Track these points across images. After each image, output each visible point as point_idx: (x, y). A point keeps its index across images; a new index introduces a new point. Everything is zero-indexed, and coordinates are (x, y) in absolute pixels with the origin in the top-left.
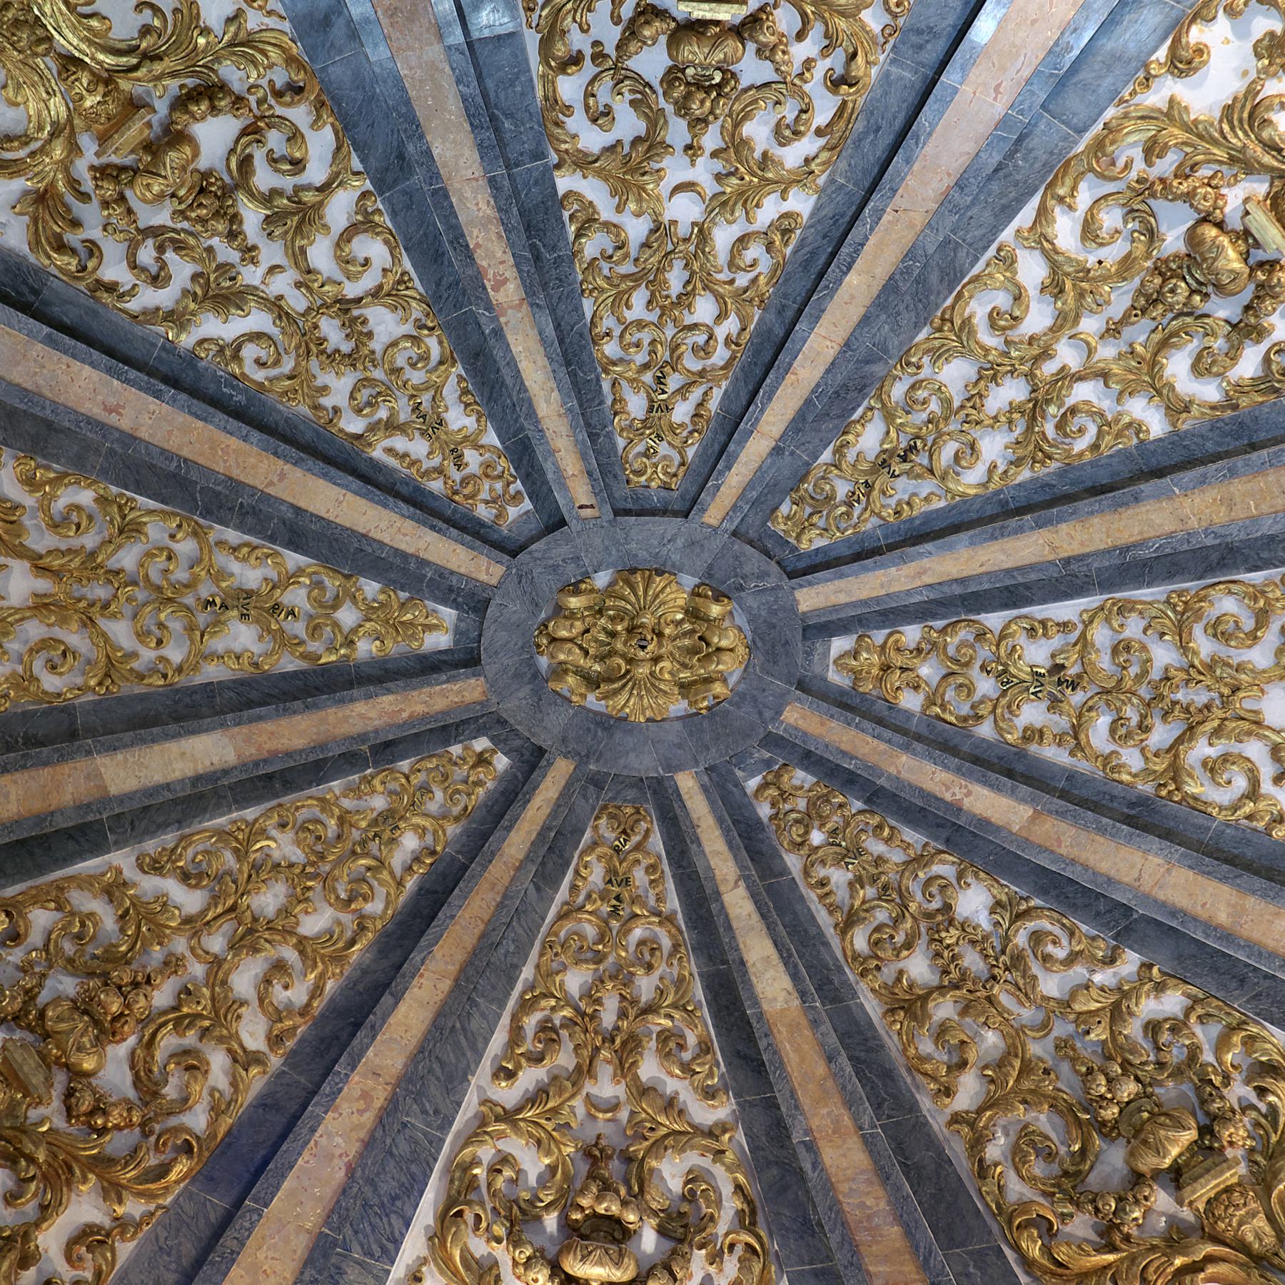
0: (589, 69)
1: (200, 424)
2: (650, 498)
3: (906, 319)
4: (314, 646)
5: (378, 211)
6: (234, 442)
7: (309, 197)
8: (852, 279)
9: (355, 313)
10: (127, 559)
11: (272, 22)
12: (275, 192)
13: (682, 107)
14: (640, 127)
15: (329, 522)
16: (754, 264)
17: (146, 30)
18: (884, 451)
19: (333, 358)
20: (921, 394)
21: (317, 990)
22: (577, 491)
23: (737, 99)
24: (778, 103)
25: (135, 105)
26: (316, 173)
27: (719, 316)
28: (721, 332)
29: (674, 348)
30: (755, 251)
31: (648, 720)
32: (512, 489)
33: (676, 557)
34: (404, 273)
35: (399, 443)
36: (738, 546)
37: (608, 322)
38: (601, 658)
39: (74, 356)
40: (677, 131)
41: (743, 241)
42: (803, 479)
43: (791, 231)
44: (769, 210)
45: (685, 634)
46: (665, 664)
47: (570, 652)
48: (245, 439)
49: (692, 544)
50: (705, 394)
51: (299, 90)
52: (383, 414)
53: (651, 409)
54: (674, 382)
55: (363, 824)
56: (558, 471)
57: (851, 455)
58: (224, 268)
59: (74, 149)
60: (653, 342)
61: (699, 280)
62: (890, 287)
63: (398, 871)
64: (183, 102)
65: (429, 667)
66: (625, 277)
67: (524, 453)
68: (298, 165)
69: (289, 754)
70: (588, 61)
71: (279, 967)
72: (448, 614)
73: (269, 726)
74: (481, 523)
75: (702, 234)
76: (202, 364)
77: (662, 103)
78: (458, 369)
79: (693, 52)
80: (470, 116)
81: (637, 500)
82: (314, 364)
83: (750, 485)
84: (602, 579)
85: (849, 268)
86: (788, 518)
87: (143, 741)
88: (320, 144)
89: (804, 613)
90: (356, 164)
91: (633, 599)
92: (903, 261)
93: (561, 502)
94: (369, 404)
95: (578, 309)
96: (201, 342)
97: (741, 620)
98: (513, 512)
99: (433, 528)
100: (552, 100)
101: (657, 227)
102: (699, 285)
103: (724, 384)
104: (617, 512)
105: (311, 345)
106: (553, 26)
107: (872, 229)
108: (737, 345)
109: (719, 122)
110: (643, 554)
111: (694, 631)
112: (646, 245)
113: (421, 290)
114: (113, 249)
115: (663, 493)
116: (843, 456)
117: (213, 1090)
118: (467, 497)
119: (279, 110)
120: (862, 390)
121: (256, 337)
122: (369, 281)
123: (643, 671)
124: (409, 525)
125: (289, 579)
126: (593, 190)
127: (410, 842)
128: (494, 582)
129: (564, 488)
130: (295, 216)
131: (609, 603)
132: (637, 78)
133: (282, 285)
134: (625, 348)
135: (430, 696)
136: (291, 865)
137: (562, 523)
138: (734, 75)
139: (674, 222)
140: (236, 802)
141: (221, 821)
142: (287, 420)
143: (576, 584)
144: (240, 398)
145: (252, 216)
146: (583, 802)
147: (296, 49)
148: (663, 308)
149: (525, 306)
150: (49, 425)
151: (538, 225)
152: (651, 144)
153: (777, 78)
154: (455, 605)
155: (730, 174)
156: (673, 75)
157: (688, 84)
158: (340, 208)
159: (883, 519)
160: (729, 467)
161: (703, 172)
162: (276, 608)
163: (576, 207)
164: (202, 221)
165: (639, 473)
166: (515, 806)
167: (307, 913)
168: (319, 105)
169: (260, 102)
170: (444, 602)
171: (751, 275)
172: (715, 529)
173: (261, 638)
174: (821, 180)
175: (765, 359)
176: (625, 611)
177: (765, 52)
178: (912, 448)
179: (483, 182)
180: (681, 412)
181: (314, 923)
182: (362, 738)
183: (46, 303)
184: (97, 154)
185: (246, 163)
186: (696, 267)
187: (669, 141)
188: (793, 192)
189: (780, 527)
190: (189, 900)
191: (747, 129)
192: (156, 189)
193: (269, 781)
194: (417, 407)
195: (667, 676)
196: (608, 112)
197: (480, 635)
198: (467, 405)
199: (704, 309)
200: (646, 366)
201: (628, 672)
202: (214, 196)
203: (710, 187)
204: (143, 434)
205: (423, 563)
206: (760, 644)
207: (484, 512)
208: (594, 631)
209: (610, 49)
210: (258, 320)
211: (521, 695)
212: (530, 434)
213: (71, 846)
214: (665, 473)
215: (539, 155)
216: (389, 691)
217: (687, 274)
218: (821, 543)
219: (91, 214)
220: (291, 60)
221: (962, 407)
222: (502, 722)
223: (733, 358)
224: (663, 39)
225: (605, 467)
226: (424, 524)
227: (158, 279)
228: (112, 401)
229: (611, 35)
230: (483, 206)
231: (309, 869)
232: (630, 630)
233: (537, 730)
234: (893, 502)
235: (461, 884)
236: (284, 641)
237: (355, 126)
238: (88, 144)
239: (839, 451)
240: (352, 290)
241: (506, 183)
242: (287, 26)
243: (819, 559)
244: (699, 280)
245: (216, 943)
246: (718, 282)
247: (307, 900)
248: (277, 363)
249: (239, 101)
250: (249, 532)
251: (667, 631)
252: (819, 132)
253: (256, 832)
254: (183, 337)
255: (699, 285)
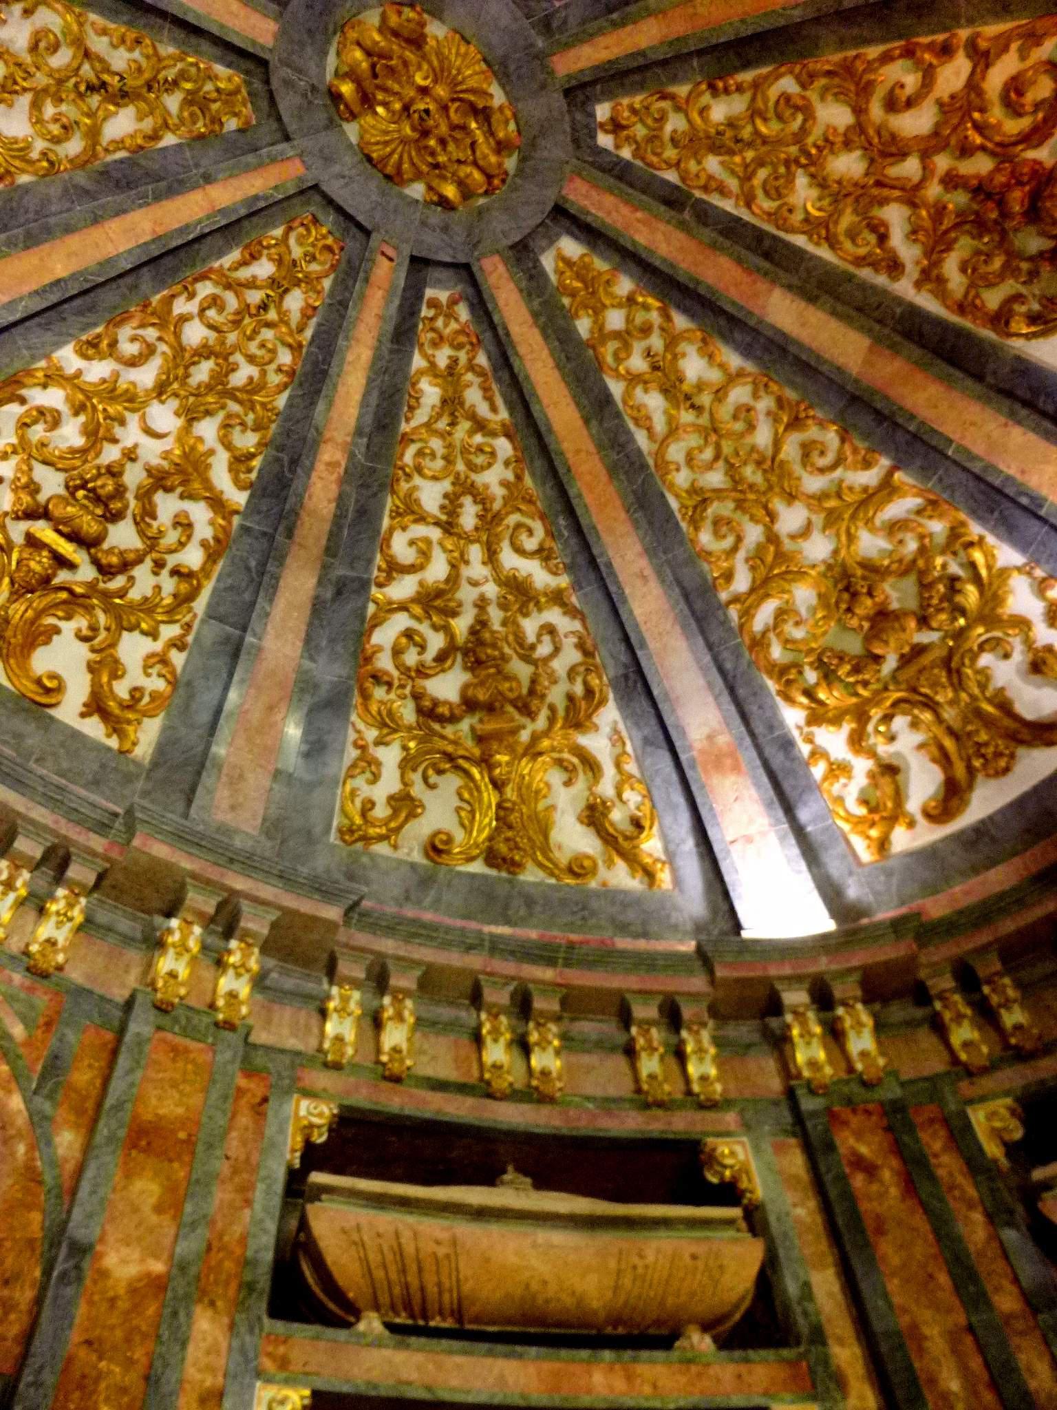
0: (172, 561)
1: (599, 527)
2: (335, 223)
3: (31, 202)
4: (655, 317)
5: (380, 569)
6: (588, 499)
7: (417, 610)
8: (60, 269)
9: (444, 518)
10: (716, 478)
11: (361, 726)
12: (435, 628)
13: (120, 492)
14: (159, 498)
15: (574, 397)
16: (133, 339)
17: (440, 772)
18: (117, 105)
19: (481, 499)
20: (56, 129)
21: (886, 58)
22: (386, 274)
23: (74, 469)
24: (44, 445)
25: (480, 739)
26: (401, 621)
27: (187, 320)
28: (192, 307)
29: (237, 323)
30: (129, 349)
31: (468, 43)
32: (431, 313)
33: (349, 159)
34: (392, 518)
35: (483, 409)
36: (292, 127)
37: (275, 379)
38: (464, 128)
39: (637, 625)
40: (134, 477)
41: (133, 362)
42: (201, 137)
43: (88, 343)
44: (97, 371)
45: (385, 90)
46: (419, 80)
47: (485, 157)
48: (580, 496)
49: (328, 160)
50: (236, 269)
51: (374, 677)
52: (478, 439)
53: (286, 291)
54: (254, 297)
55: (737, 159)
56: (388, 301)
57: (148, 124)
58: (504, 606)
59: (535, 738)
60: (250, 339)
61: (183, 359)
62: (31, 241)
63: (748, 96)
64: (453, 719)
65: (591, 234)
66: (240, 402)
67: (403, 334)
68: (409, 634)
69: (739, 261)
70: (170, 566)
71: (892, 105)
72: (548, 262)
73: (733, 294)
74: (472, 308)
75: (160, 390)
76: (567, 561)
77: (133, 503)
78: (404, 427)
79: (89, 525)
80: (275, 588)
81: (346, 230)
82: (497, 505)
83: (248, 169)
84: (417, 190)
85: (58, 281)
86: (236, 115)
87: (818, 357)
88: (385, 636)
89: (275, 20)
90: (371, 608)
91: (405, 157)
92: (9, 255)
93: (403, 275)
94: (482, 451)
95: (290, 405)
96: (555, 574)
97: (331, 61)
98: (443, 296)
99: (508, 334)
100: (212, 556)
101: (191, 421)
102: (187, 355)
103: (216, 265)
104: (367, 233)
105: (489, 520)
106: (179, 605)
107: (21, 299)
108: (186, 288)
109: (98, 461)
110: (373, 185)
111: (378, 87)
112: (208, 413)
113: (389, 499)
114: (560, 666)
115: (320, 217)
116: (155, 131)
117: (1023, 57)
118: (468, 335)
119: (395, 673)
120: (105, 173)
121: (520, 551)
122: (419, 530)
123: (441, 91)
124: (522, 350)
125: (634, 379)
126: (221, 476)
127: (720, 111)
128: (496, 258)
129: (393, 287)
130: (435, 603)
131: (424, 168)
132: (142, 534)
133: (476, 568)
134: (273, 352)
135: (609, 213)
136: (813, 176)
137: (414, 260)
138: (67, 487)
139: (177, 414)
140: (802, 259)
141: (824, 253)
142: (544, 484)
143: (438, 204)
144: (562, 522)
145: (461, 625)
146: (571, 20)
147: (356, 699)
148: (226, 359)
149: (327, 435)
150: (686, 596)
151: (277, 488)
152: (159, 480)
153: (34, 462)
154: (537, 263)
155: (113, 419)
156: (115, 517)
157: (106, 506)
158: (403, 589)
159: (154, 47)
160: (256, 198)
161: (131, 434)
162: (655, 368)
163: (242, 476)
164: (494, 646)
165: (329, 249)
166: (623, 66)
167: (835, 129)
168: (368, 660)
169: (402, 686)
170: (543, 274)
171: (140, 332)
172: (300, 156)
173: (684, 355)
174: (43, 364)
175: (173, 260)
176: (419, 150)
177: (33, 488)
178: (91, 88)
179: (297, 539)
180: (264, 269)
181: (834, 115)
182: (682, 226)
183: (626, 666)
184: (524, 727)
185: (441, 658)
186: (181, 372)
187: (145, 474)
188: (70, 371)
189: (247, 110)
190: (895, 216)
191: (79, 441)
192: (507, 685)
193: (767, 252)
194: (453, 424)
195: (425, 66)
196: (176, 524)
197: (538, 226)
198: (417, 399)
199: (195, 334)
200: (269, 325)
201: (453, 100)
202: (476, 652)
203: (133, 420)
204: (638, 548)
205: (535, 315)
206: (331, 28)
207: (463, 312)
208: (455, 157)
209: (148, 563)
210: (509, 559)
211: (546, 154)
212: (389, 345)
213: (926, 328)
214: (308, 230)
215: (245, 530)
216: (634, 242)
217: (192, 370)
218: (220, 69)
219: (556, 695)
220: (366, 696)
221: (25, 90)
222: (576, 142)
223: (196, 280)
224: (105, 546)
225: (351, 273)
226: (511, 342)
227: (550, 630)
228: (638, 583)
229: (142, 573)
230: (307, 525)
231: (803, 161)
232: (425, 133)
233: (555, 114)
234: (136, 54)
235: (714, 41)
236: (672, 341)
237: (354, 632)
238: (525, 736)
239: (155, 137)
240: (435, 534)
241: (281, 529)
242: (354, 717)
243: (232, 57)
244: (183, 359)
245: (910, 167)
246: (172, 347)
247: (826, 140)
248: (519, 526)
249: (417, 697)
250: (628, 433)
251: (397, 106)
252: (23, 401)
253: (810, 226)
254: (564, 585)
255: (187, 355)
